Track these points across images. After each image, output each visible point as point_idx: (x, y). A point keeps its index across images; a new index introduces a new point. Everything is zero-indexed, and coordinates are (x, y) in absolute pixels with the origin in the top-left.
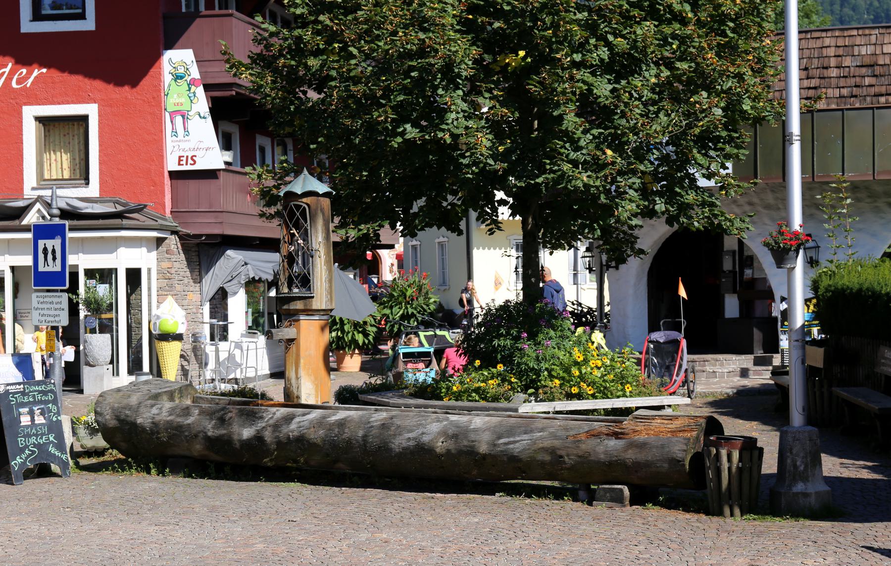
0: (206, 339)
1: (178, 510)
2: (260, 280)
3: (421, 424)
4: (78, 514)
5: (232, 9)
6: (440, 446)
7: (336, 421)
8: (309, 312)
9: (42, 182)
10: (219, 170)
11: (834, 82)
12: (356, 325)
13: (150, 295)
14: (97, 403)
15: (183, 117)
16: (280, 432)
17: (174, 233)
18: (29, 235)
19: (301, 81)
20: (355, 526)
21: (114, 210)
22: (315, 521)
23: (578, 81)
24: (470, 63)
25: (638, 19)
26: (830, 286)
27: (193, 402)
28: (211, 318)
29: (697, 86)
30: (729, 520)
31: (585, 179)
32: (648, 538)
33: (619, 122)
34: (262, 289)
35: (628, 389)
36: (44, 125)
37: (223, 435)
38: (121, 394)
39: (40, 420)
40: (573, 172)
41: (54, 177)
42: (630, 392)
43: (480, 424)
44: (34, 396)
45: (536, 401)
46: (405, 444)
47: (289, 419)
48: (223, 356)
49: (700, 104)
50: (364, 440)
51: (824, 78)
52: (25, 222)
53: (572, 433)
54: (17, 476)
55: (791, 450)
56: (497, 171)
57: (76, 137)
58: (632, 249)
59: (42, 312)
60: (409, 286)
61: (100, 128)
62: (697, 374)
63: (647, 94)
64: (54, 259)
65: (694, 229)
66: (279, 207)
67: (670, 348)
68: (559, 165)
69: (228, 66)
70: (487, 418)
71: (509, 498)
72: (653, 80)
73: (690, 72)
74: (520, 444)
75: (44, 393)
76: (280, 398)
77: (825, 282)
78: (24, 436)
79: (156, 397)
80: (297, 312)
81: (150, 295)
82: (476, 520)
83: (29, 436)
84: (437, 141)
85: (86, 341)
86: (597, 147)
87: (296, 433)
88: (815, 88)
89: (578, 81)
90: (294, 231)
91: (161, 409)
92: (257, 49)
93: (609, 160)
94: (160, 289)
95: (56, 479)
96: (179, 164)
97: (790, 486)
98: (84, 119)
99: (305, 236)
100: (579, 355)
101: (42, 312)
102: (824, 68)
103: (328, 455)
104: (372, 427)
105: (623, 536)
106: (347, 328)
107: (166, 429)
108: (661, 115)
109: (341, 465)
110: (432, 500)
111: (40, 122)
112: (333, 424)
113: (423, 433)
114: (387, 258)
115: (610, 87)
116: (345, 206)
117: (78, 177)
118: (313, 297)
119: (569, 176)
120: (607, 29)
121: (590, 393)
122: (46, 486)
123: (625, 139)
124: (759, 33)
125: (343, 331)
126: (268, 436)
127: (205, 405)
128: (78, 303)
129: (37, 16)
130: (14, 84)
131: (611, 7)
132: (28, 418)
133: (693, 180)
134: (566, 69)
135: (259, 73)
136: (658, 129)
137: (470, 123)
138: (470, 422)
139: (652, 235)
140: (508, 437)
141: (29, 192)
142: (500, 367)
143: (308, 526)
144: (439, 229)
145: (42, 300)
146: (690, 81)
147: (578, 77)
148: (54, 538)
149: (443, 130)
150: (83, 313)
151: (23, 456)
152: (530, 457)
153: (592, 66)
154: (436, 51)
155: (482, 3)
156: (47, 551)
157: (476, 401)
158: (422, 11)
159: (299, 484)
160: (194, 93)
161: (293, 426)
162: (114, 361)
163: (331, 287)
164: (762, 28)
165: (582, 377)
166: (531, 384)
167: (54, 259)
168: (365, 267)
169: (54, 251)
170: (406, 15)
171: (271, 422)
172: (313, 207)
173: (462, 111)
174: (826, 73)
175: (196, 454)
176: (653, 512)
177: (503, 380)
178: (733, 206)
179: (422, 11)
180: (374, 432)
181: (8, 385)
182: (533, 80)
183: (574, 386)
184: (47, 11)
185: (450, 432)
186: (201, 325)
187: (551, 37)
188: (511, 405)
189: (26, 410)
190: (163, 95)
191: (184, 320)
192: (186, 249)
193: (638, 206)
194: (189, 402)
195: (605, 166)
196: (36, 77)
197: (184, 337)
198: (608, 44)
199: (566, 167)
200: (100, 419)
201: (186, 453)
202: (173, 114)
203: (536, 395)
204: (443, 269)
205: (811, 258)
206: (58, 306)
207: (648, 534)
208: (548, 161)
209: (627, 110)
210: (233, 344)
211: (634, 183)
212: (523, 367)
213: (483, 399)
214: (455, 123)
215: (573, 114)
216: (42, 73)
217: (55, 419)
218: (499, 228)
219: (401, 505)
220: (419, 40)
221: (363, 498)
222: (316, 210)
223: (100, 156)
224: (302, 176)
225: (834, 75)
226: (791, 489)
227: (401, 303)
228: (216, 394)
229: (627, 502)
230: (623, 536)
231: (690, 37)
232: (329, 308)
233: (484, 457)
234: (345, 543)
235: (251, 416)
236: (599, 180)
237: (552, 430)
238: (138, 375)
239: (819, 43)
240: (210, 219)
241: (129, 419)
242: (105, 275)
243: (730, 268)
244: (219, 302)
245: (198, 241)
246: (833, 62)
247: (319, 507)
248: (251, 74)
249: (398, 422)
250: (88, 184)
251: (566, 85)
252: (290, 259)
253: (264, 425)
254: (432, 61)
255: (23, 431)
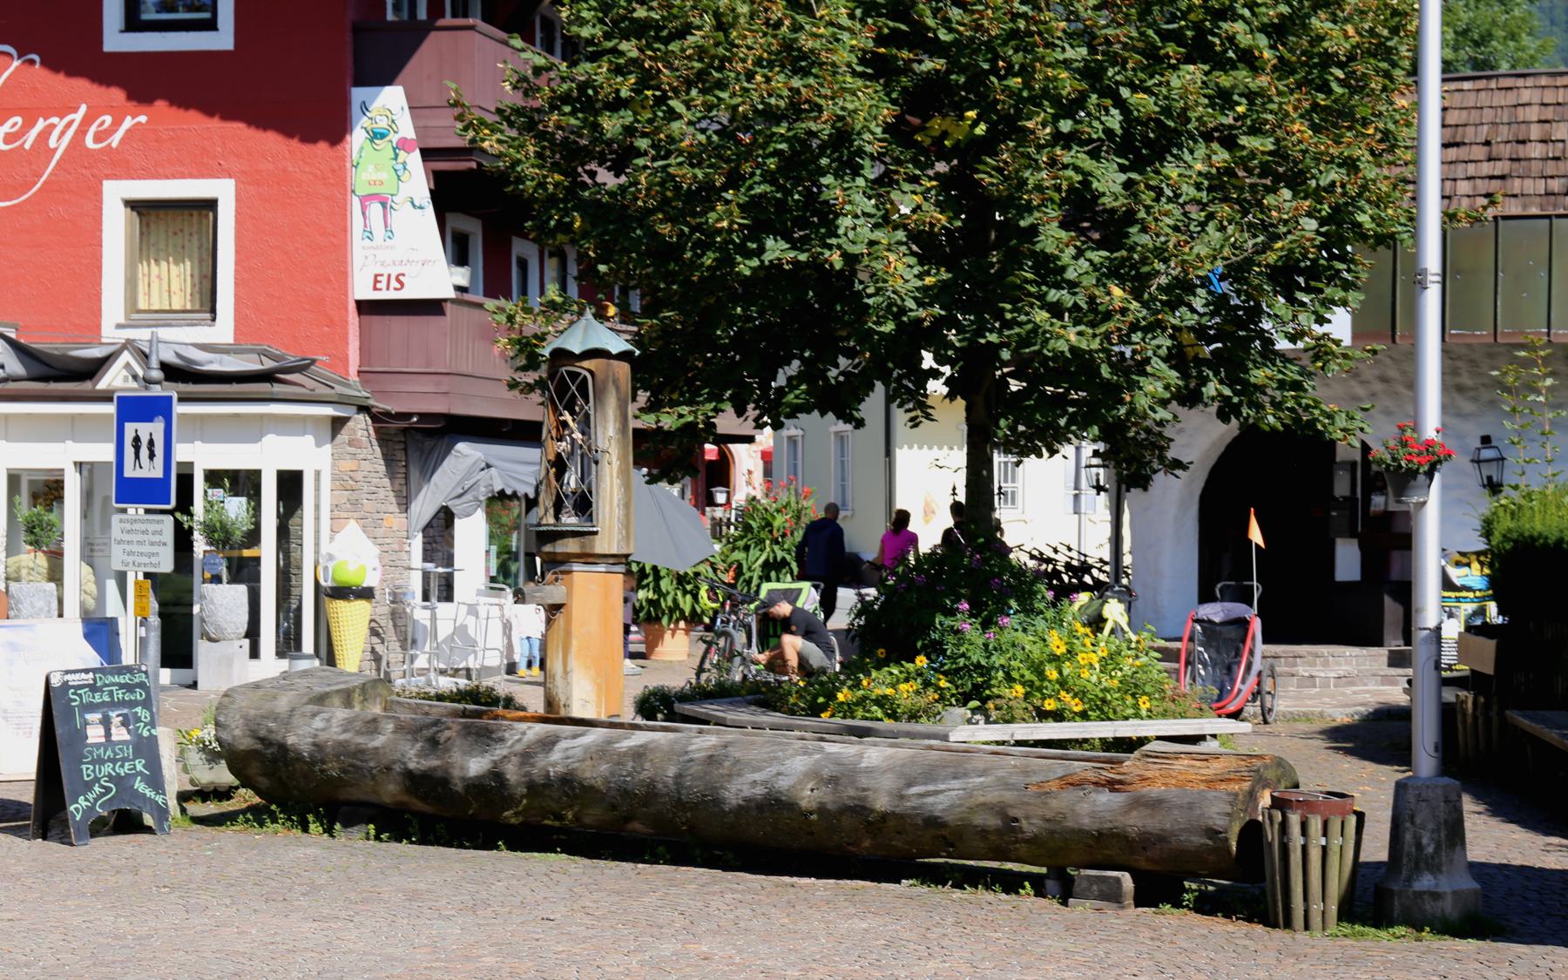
0: (416, 601)
1: (352, 896)
2: (515, 495)
3: (775, 758)
4: (181, 897)
5: (474, 17)
6: (808, 797)
7: (631, 748)
8: (588, 558)
9: (135, 314)
10: (445, 300)
11: (1536, 167)
12: (681, 580)
13: (317, 518)
14: (220, 708)
15: (384, 205)
16: (533, 765)
17: (363, 409)
18: (110, 409)
19: (584, 155)
20: (655, 931)
21: (258, 367)
22: (587, 920)
23: (1065, 167)
24: (879, 130)
25: (1173, 61)
26: (1510, 530)
27: (385, 709)
28: (425, 560)
29: (1278, 178)
30: (1302, 936)
31: (1073, 338)
32: (1158, 963)
33: (1136, 239)
34: (516, 512)
35: (1144, 704)
36: (140, 214)
37: (435, 769)
38: (260, 692)
39: (120, 734)
40: (1052, 324)
41: (156, 307)
42: (1149, 710)
43: (878, 765)
44: (111, 694)
45: (987, 722)
46: (747, 792)
47: (548, 744)
48: (444, 630)
49: (1279, 210)
50: (676, 784)
51: (1518, 160)
52: (103, 384)
53: (1035, 779)
54: (78, 830)
55: (1412, 818)
56: (920, 320)
57: (195, 238)
58: (1162, 458)
59: (128, 548)
60: (778, 511)
61: (238, 222)
62: (1279, 680)
63: (1188, 191)
64: (152, 456)
65: (1267, 429)
66: (543, 372)
67: (1231, 632)
68: (1027, 314)
69: (460, 125)
70: (890, 751)
71: (925, 889)
72: (1199, 166)
73: (1263, 153)
74: (945, 798)
75: (129, 688)
76: (536, 705)
77: (1505, 523)
78: (93, 762)
79: (321, 699)
80: (567, 558)
81: (317, 518)
82: (865, 925)
83: (101, 761)
84: (816, 264)
85: (203, 597)
86: (1099, 283)
87: (560, 769)
88: (1503, 177)
89: (1065, 167)
90: (567, 417)
91: (328, 720)
92: (517, 100)
93: (1117, 304)
94: (336, 507)
95: (146, 837)
96: (375, 289)
97: (1409, 880)
98: (211, 205)
99: (586, 424)
100: (1058, 642)
101: (128, 548)
102: (1518, 142)
103: (614, 807)
104: (691, 760)
105: (1114, 958)
106: (665, 584)
107: (337, 756)
108: (1211, 228)
109: (636, 826)
110: (792, 890)
111: (133, 208)
112: (625, 754)
113: (779, 774)
114: (746, 459)
115: (1123, 177)
116: (656, 371)
117: (197, 307)
118: (596, 533)
119: (1045, 332)
120: (1118, 78)
121: (1076, 709)
122: (129, 849)
123: (1146, 269)
124: (1384, 89)
125: (657, 589)
126: (512, 772)
127: (405, 716)
128: (191, 529)
129: (133, 23)
130: (89, 142)
131: (1123, 39)
132: (101, 731)
133: (1268, 343)
134: (1044, 146)
135: (514, 139)
136: (1203, 254)
137: (880, 238)
138: (861, 756)
139: (1200, 437)
140: (925, 784)
141: (112, 329)
142: (921, 661)
143: (574, 929)
144: (823, 414)
145: (128, 526)
146: (1266, 170)
147: (1066, 160)
148: (140, 938)
149: (830, 247)
150: (200, 546)
151: (91, 796)
152: (961, 819)
153: (1091, 141)
154: (820, 109)
155: (903, 27)
156: (128, 960)
157: (878, 719)
158: (796, 40)
159: (564, 856)
160: (404, 164)
161: (556, 755)
162: (253, 633)
163: (632, 511)
164: (1392, 80)
165: (1063, 683)
166: (976, 692)
167: (152, 456)
168: (702, 476)
169: (151, 443)
170: (770, 44)
171: (519, 748)
172: (599, 376)
173: (864, 214)
174: (1522, 151)
175: (387, 800)
176: (1171, 921)
177: (927, 684)
178: (1353, 383)
179: (796, 40)
180: (695, 769)
181: (67, 672)
182: (986, 164)
183: (1050, 697)
184: (149, 15)
185: (826, 773)
186: (406, 573)
187: (1021, 90)
188: (938, 728)
189: (98, 716)
190: (348, 165)
191: (377, 563)
192: (383, 439)
193: (1167, 387)
194: (377, 710)
195: (1108, 316)
196: (128, 131)
197: (377, 593)
198: (1121, 104)
199: (1041, 316)
200: (224, 736)
201: (373, 798)
202: (365, 200)
203: (981, 710)
204: (843, 479)
205: (1490, 478)
206: (156, 538)
207: (1159, 956)
208: (1008, 306)
209: (1150, 219)
210: (464, 609)
211: (1159, 347)
212: (962, 661)
213: (889, 716)
214: (851, 234)
215: (1056, 224)
216: (139, 123)
217: (145, 734)
218: (928, 417)
219: (738, 896)
220: (791, 89)
221: (672, 883)
222: (605, 382)
223: (236, 271)
224: (583, 321)
225: (1536, 154)
226: (1410, 886)
227: (762, 541)
228: (427, 697)
229: (1130, 901)
230: (1114, 958)
231: (1261, 93)
232: (624, 552)
233: (884, 817)
234: (634, 961)
235: (484, 738)
236: (1098, 340)
237: (1000, 773)
238: (293, 658)
239: (1511, 98)
240: (426, 385)
241: (273, 737)
242: (244, 483)
243: (1347, 493)
244: (440, 529)
245: (403, 424)
246: (1535, 132)
247: (596, 896)
248: (499, 141)
249: (735, 752)
250: (214, 319)
251: (1044, 174)
252: (559, 465)
253: (505, 752)
254: (814, 127)
255: (91, 753)
